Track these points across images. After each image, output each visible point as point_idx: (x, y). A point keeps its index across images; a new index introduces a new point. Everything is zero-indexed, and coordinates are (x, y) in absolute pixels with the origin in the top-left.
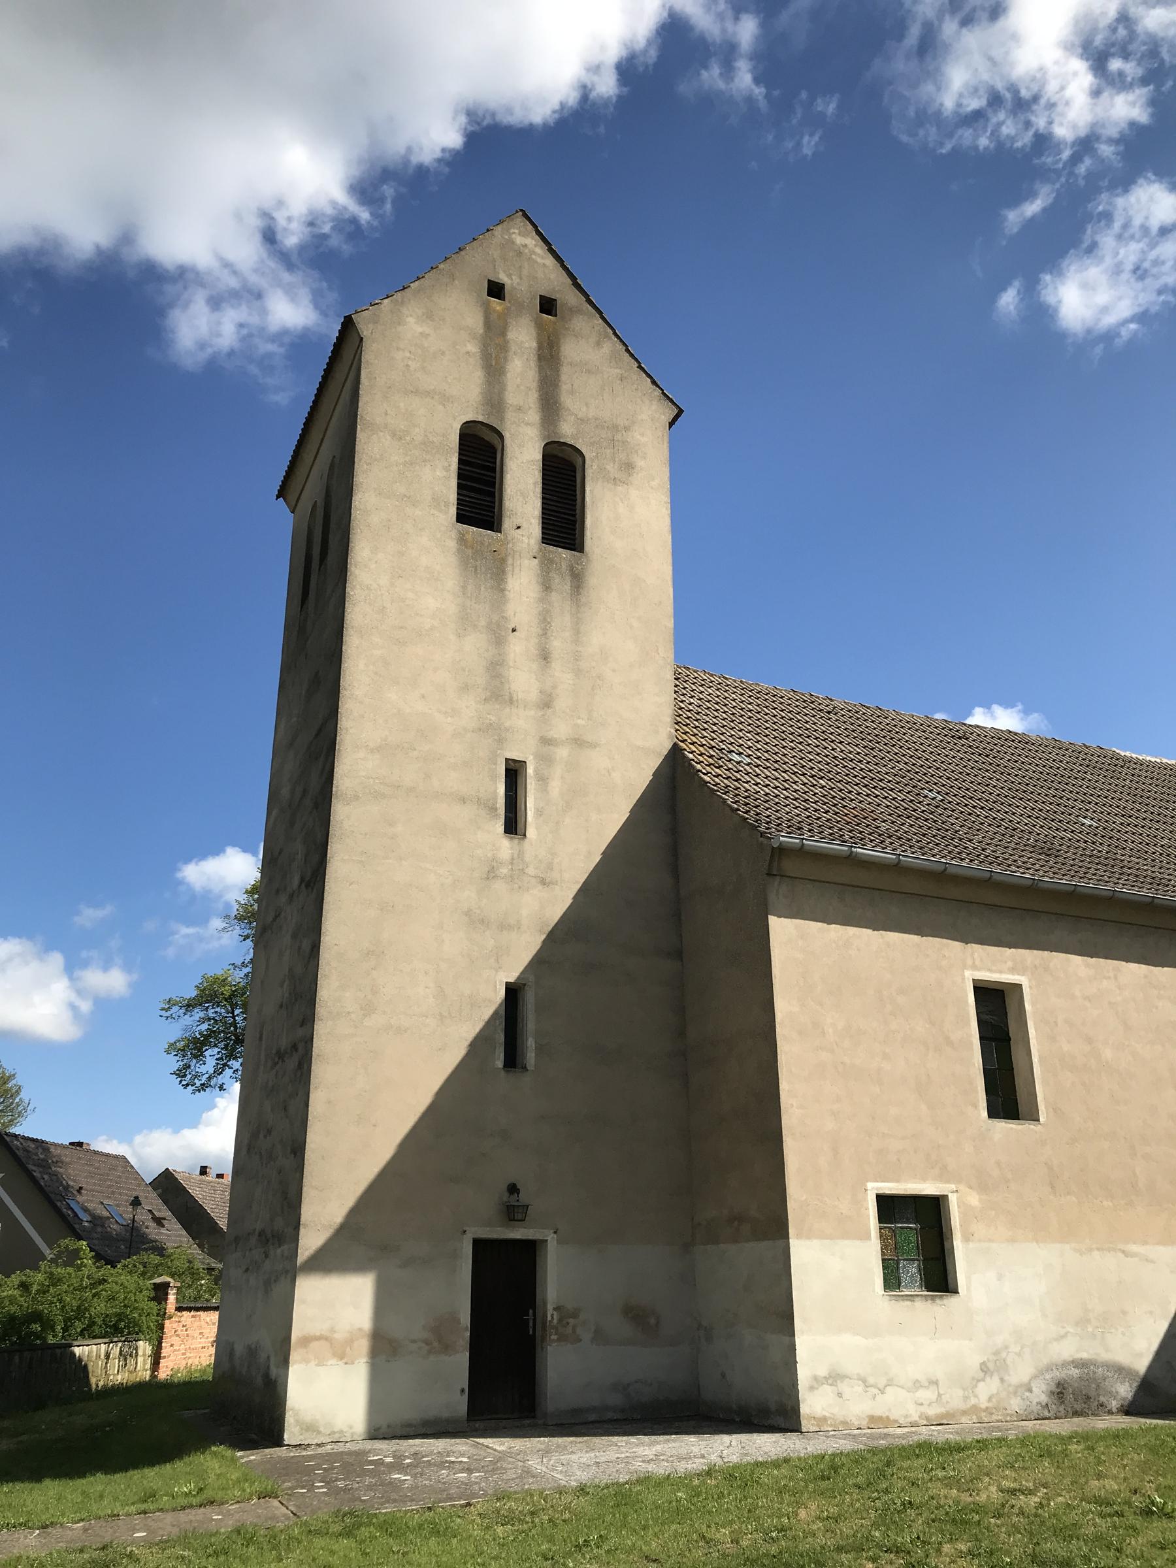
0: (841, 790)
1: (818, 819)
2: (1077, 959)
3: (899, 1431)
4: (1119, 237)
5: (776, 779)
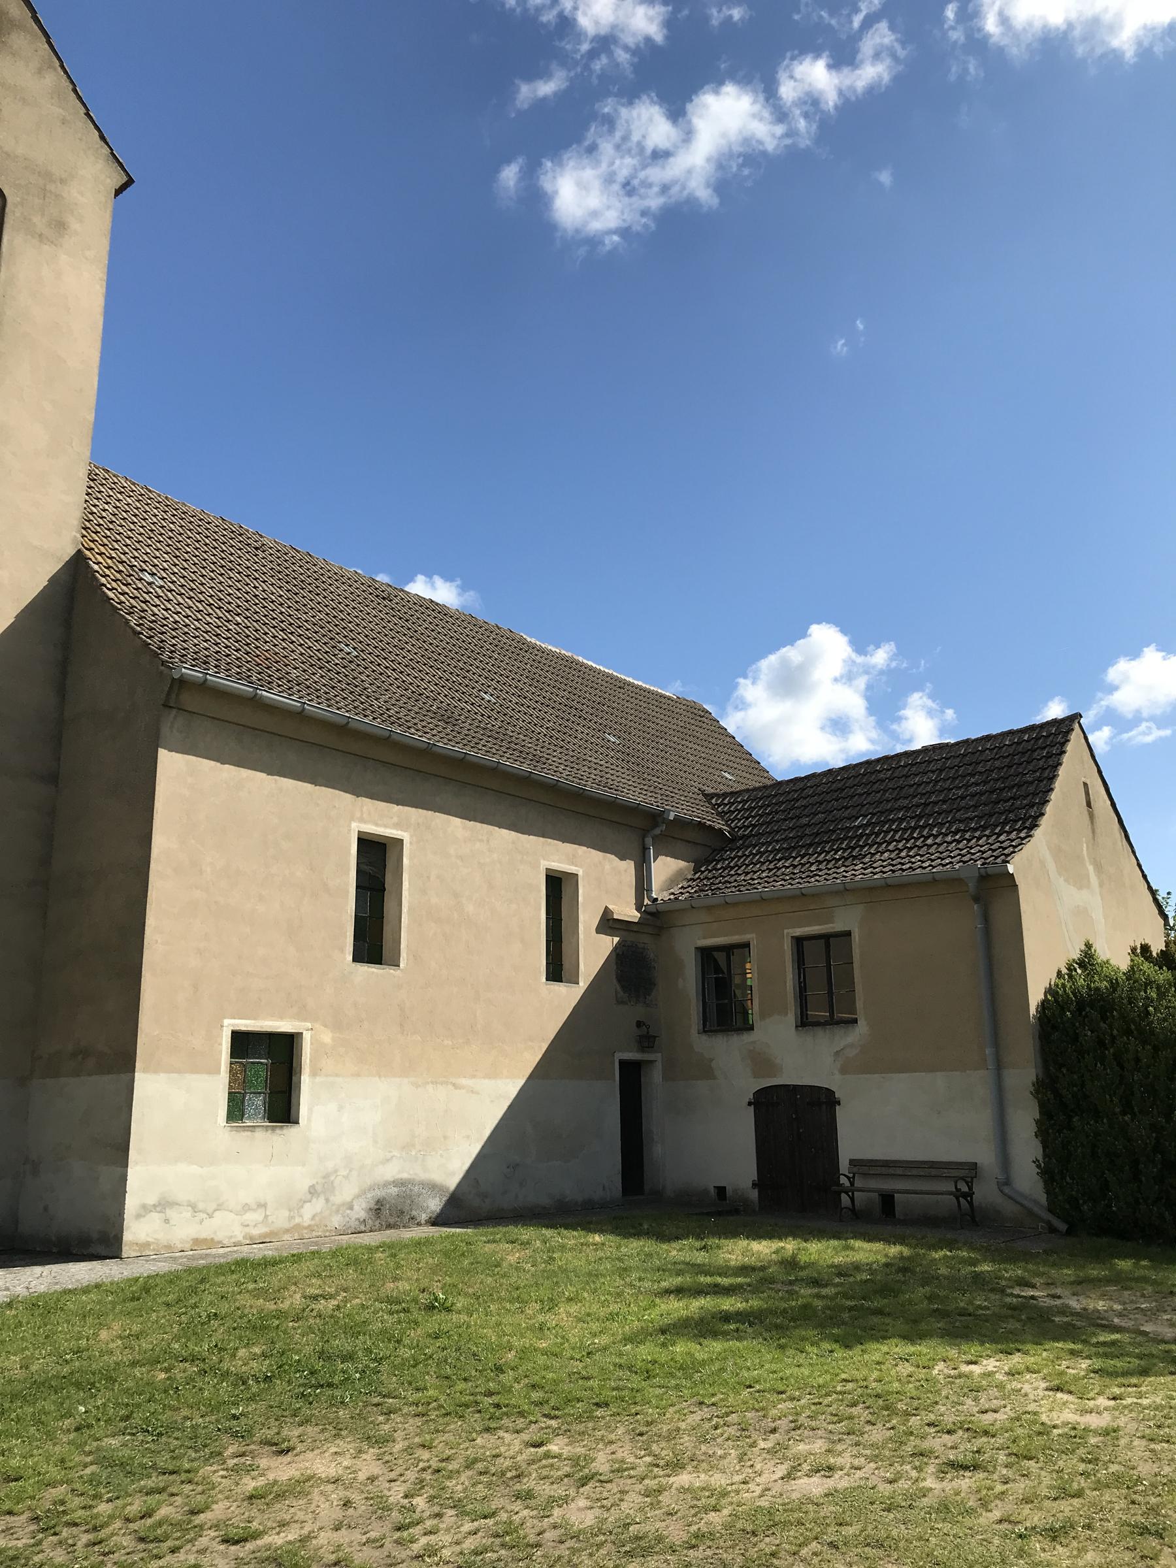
0: (256, 631)
1: (228, 656)
2: (457, 821)
3: (222, 1251)
4: (618, 147)
5: (189, 608)
